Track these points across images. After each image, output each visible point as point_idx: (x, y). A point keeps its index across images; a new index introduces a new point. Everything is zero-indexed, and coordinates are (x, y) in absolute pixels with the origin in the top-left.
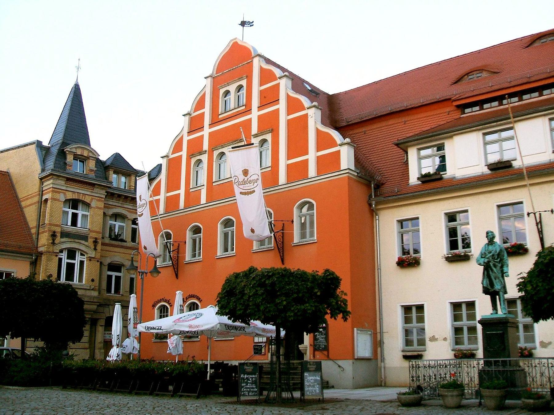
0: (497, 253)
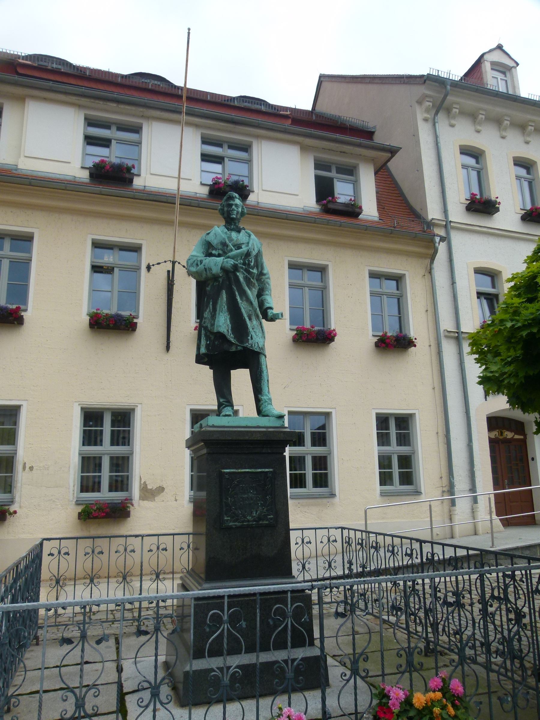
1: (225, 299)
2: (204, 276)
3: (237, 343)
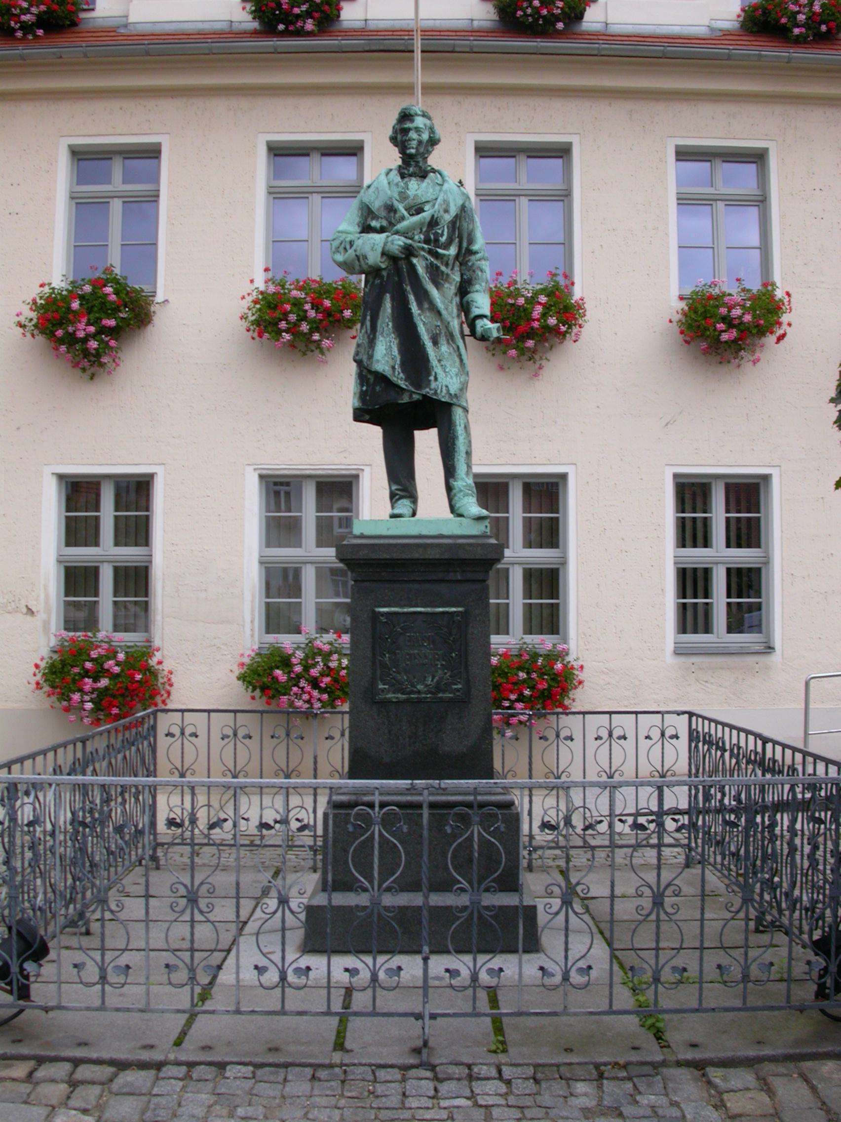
0: (448, 218)
1: (389, 311)
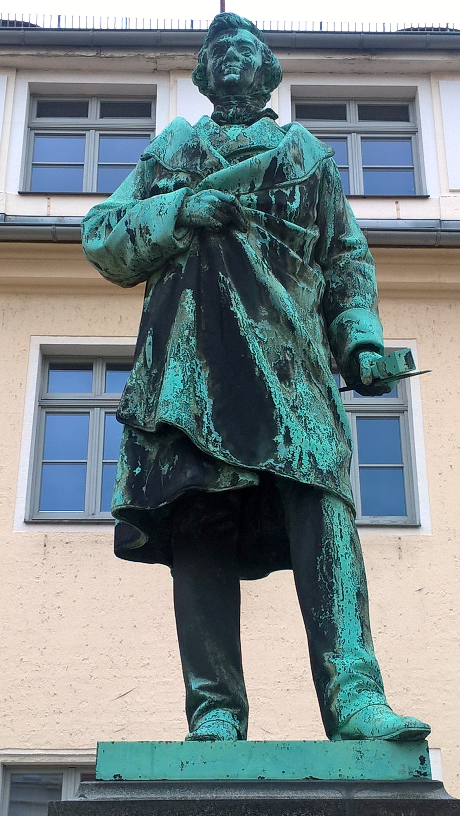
2: (130, 256)
3: (234, 460)
